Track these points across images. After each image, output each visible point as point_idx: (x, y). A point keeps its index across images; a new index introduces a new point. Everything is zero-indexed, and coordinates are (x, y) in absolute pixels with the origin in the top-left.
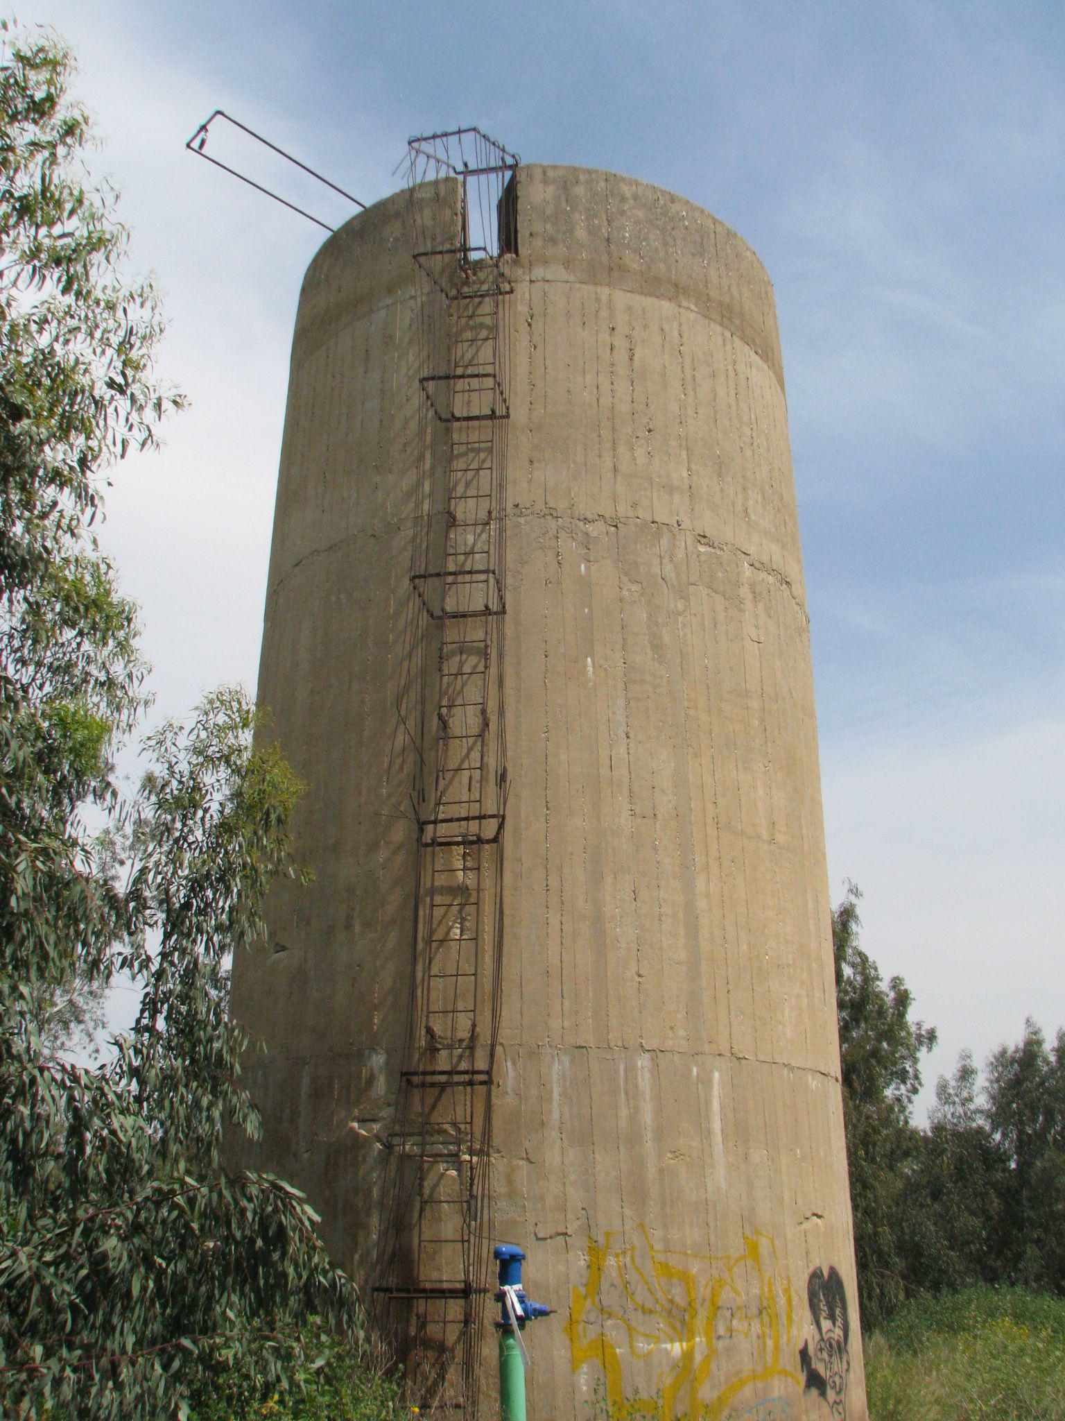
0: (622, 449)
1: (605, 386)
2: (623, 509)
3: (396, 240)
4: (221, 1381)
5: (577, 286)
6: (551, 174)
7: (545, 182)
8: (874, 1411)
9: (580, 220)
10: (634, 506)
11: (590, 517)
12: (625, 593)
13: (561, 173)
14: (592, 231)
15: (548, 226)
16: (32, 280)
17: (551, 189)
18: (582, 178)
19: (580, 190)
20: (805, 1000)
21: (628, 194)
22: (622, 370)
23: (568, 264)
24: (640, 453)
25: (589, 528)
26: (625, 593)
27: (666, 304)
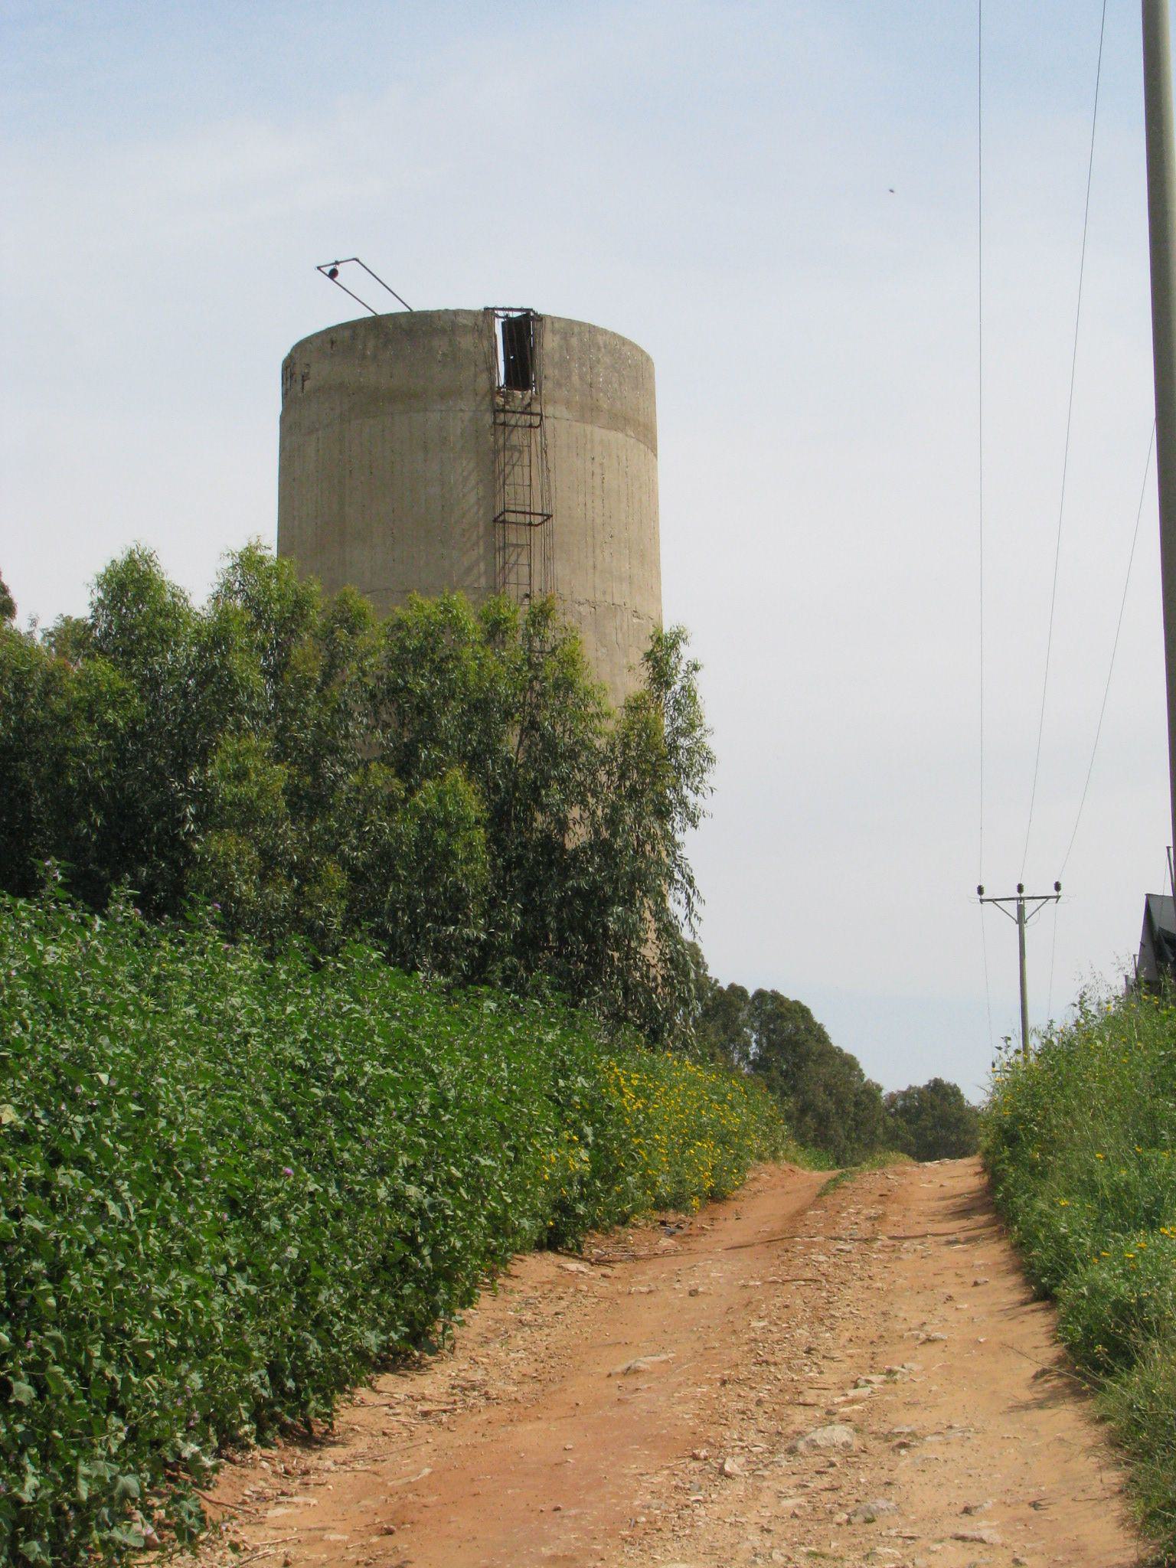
0: (598, 551)
1: (589, 503)
2: (599, 596)
3: (444, 354)
4: (373, 1292)
5: (574, 423)
6: (556, 325)
7: (553, 332)
8: (526, 742)
9: (575, 365)
10: (604, 593)
11: (582, 601)
12: (599, 654)
13: (563, 325)
14: (581, 378)
15: (556, 372)
16: (943, 1199)
17: (557, 338)
18: (576, 330)
19: (574, 341)
20: (538, 1146)
21: (601, 343)
22: (598, 492)
23: (568, 404)
24: (606, 553)
25: (581, 609)
26: (599, 654)
27: (620, 435)
